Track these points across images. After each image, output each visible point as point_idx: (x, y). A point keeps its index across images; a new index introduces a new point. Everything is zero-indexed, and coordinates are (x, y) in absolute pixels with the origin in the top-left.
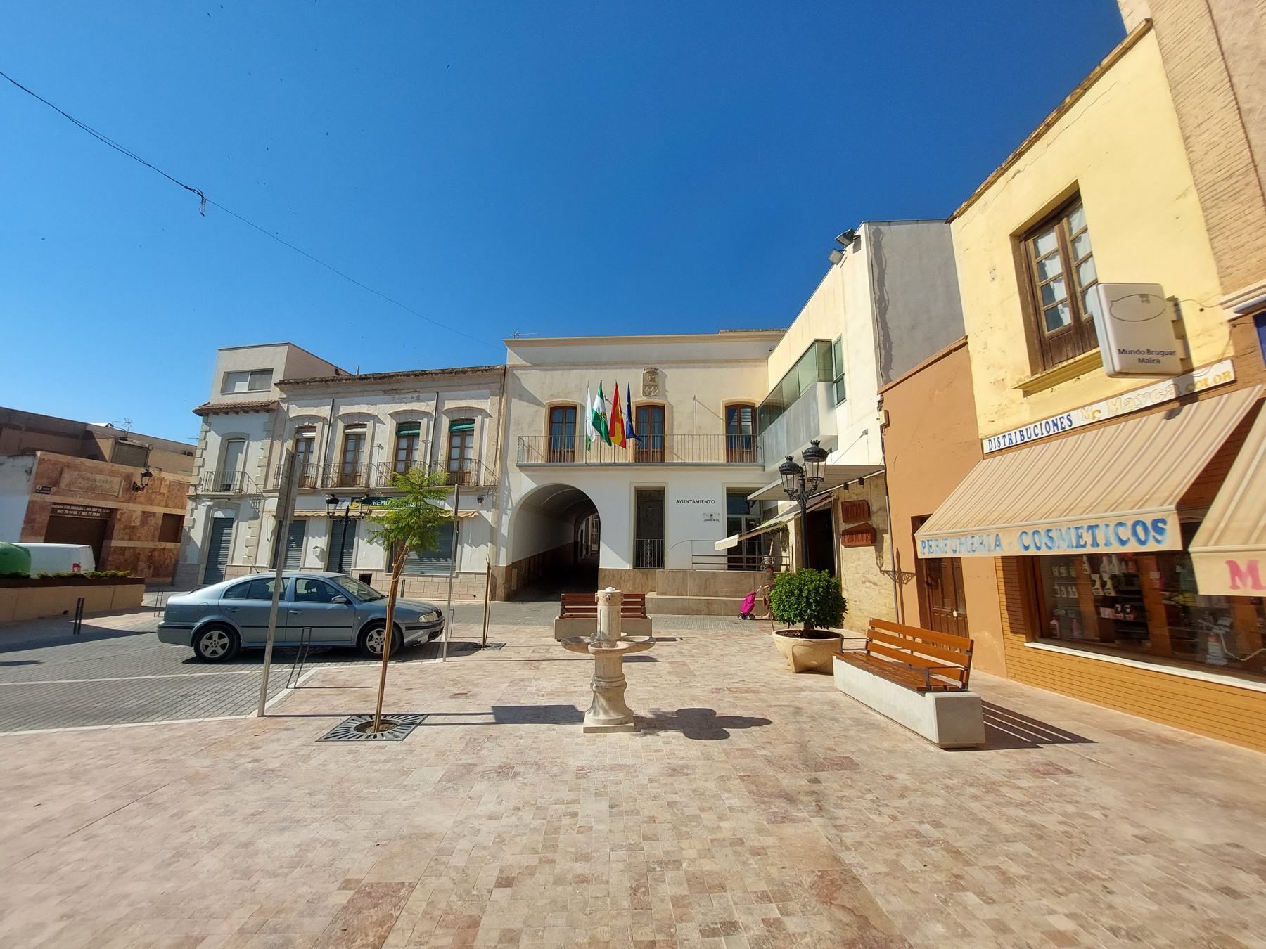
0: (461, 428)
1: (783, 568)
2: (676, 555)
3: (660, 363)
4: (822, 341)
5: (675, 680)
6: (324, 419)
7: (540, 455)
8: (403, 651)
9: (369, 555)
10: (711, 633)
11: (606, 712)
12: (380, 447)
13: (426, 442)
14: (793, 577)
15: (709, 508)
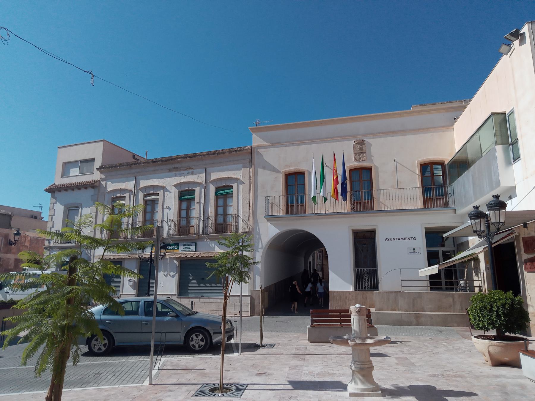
0: (224, 192)
1: (477, 290)
2: (388, 278)
3: (366, 135)
4: (498, 114)
5: (402, 368)
6: (131, 191)
7: (280, 209)
8: (211, 348)
9: (166, 285)
10: (422, 338)
11: (363, 383)
12: (169, 208)
13: (199, 203)
14: (485, 297)
15: (411, 244)
